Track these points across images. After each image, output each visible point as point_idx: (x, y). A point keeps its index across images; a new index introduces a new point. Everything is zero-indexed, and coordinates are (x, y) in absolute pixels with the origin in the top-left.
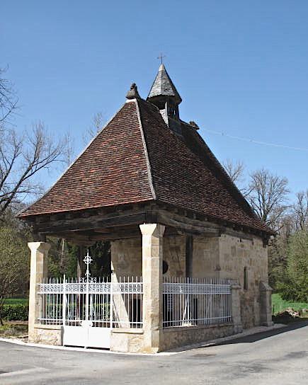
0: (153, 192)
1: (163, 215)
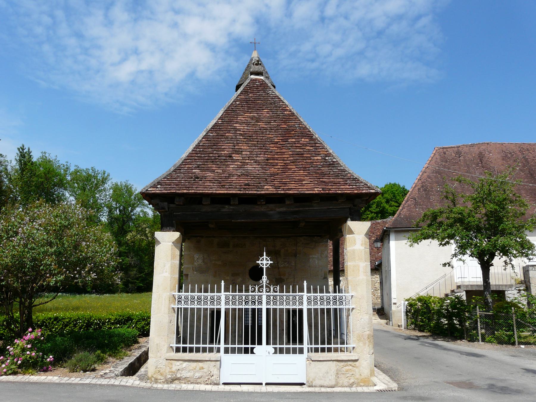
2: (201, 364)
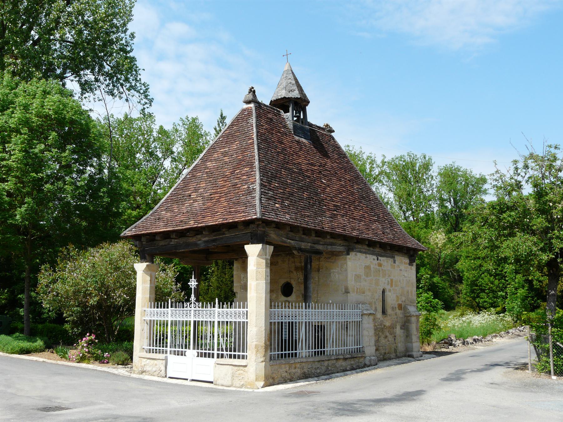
0: (258, 210)
1: (273, 235)
2: (156, 362)
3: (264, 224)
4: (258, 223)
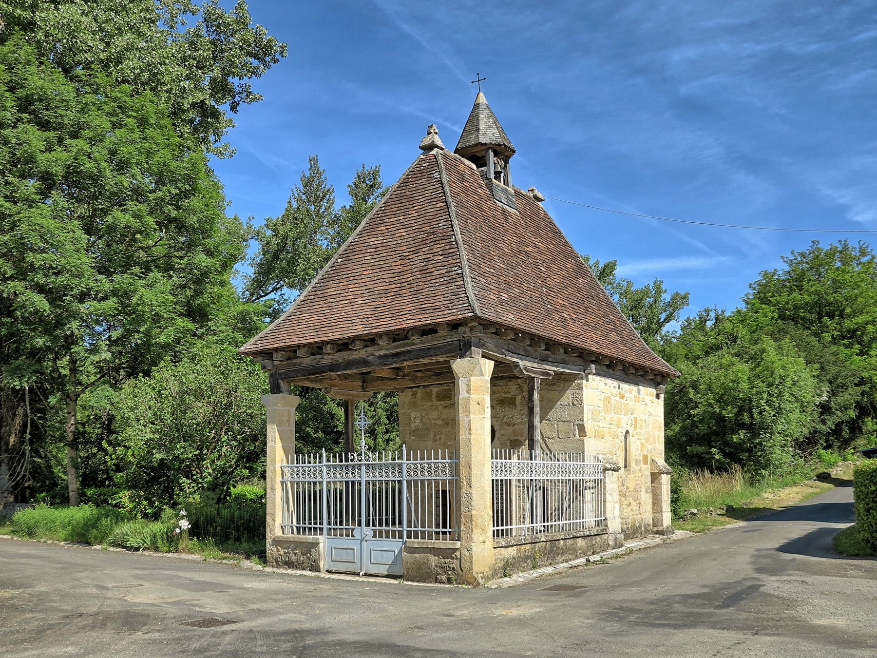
3: (481, 327)
4: (473, 324)
